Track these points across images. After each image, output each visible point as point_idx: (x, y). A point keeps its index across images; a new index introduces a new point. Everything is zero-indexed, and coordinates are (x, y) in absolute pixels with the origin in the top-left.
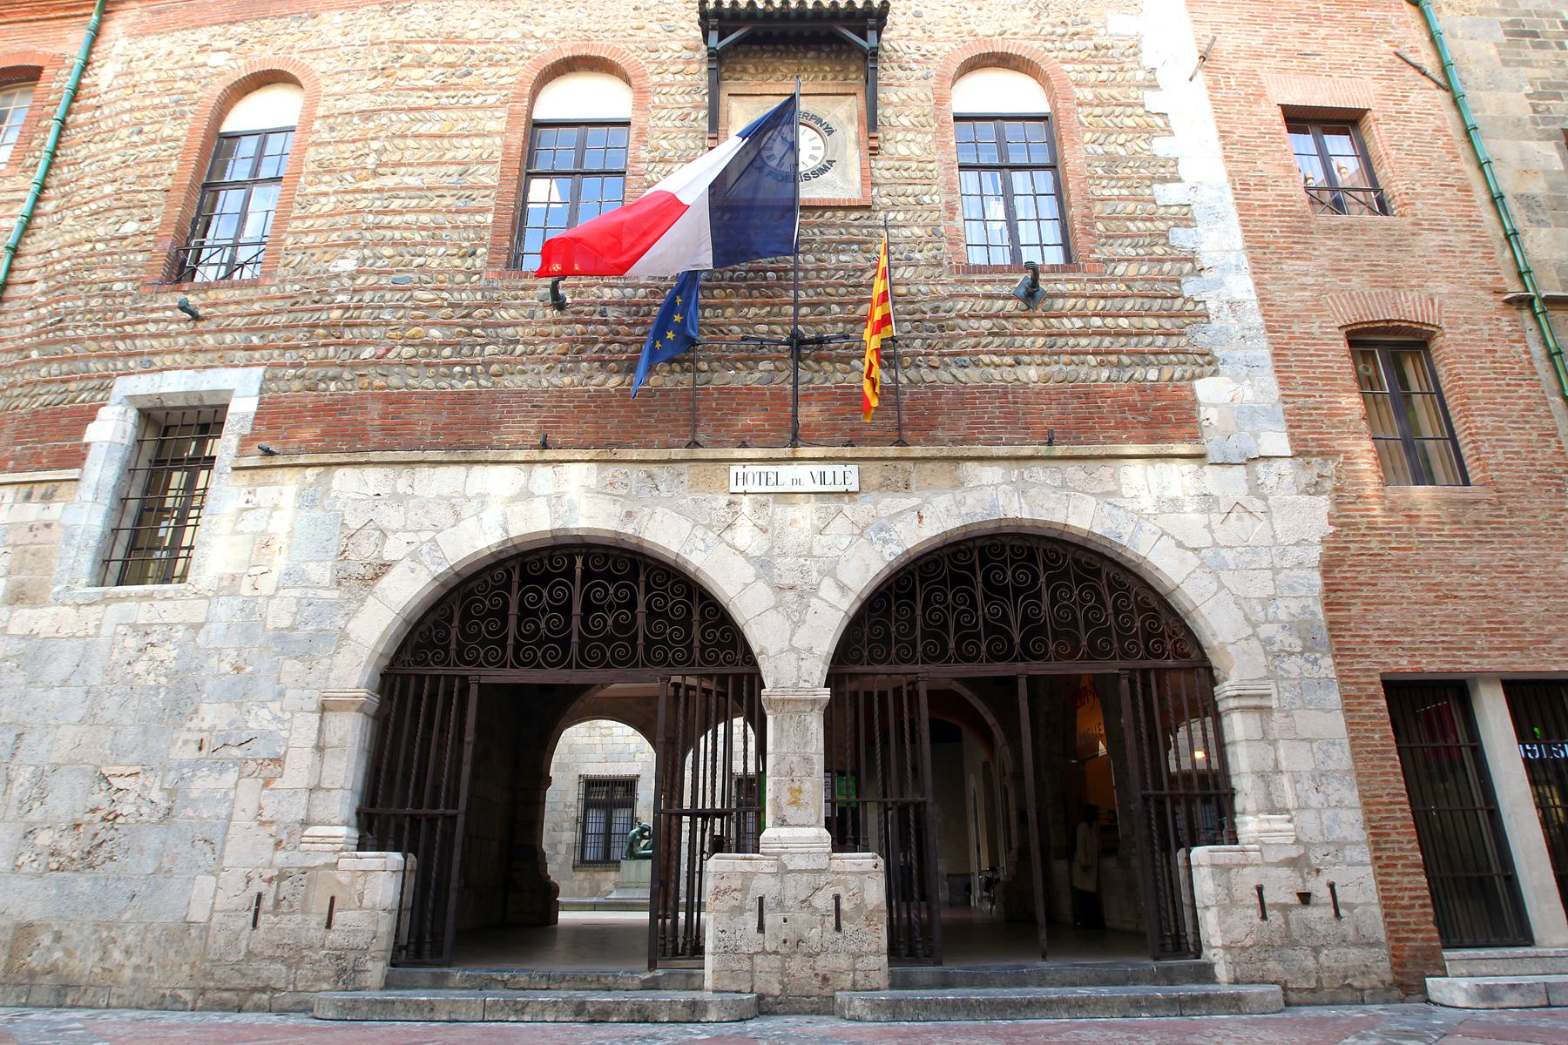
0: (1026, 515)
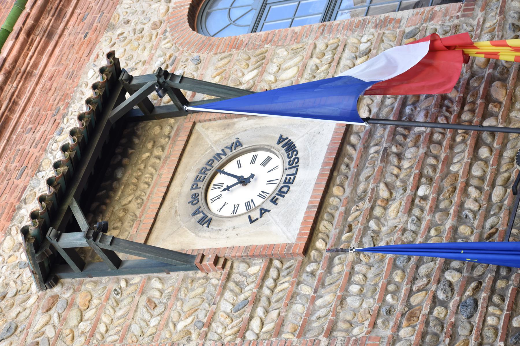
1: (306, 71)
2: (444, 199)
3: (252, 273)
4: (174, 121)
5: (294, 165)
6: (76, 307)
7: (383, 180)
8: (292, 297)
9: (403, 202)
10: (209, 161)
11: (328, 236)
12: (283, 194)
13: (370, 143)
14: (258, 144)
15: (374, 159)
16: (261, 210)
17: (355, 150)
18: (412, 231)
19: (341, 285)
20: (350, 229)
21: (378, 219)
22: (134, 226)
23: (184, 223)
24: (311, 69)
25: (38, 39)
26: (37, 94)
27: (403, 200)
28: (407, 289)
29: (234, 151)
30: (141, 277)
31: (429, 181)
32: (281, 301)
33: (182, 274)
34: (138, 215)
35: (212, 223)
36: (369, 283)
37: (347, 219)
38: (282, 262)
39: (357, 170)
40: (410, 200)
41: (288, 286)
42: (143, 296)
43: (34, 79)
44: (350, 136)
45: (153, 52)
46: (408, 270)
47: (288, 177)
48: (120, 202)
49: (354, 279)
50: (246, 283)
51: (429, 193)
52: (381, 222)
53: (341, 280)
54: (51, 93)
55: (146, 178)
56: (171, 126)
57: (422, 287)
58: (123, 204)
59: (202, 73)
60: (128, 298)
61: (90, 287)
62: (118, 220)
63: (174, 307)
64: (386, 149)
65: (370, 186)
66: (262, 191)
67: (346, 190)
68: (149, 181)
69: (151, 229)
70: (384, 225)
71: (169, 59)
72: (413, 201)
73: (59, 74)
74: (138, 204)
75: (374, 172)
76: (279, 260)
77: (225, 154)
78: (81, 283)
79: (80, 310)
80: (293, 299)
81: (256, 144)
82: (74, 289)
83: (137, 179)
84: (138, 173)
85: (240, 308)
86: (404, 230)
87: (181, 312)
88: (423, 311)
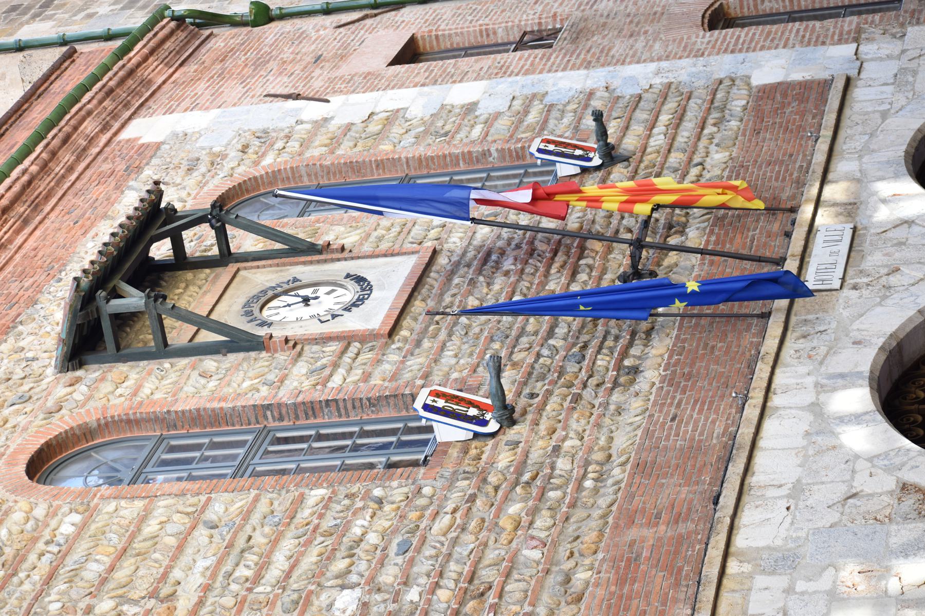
0: (904, 148)
25: (12, 220)
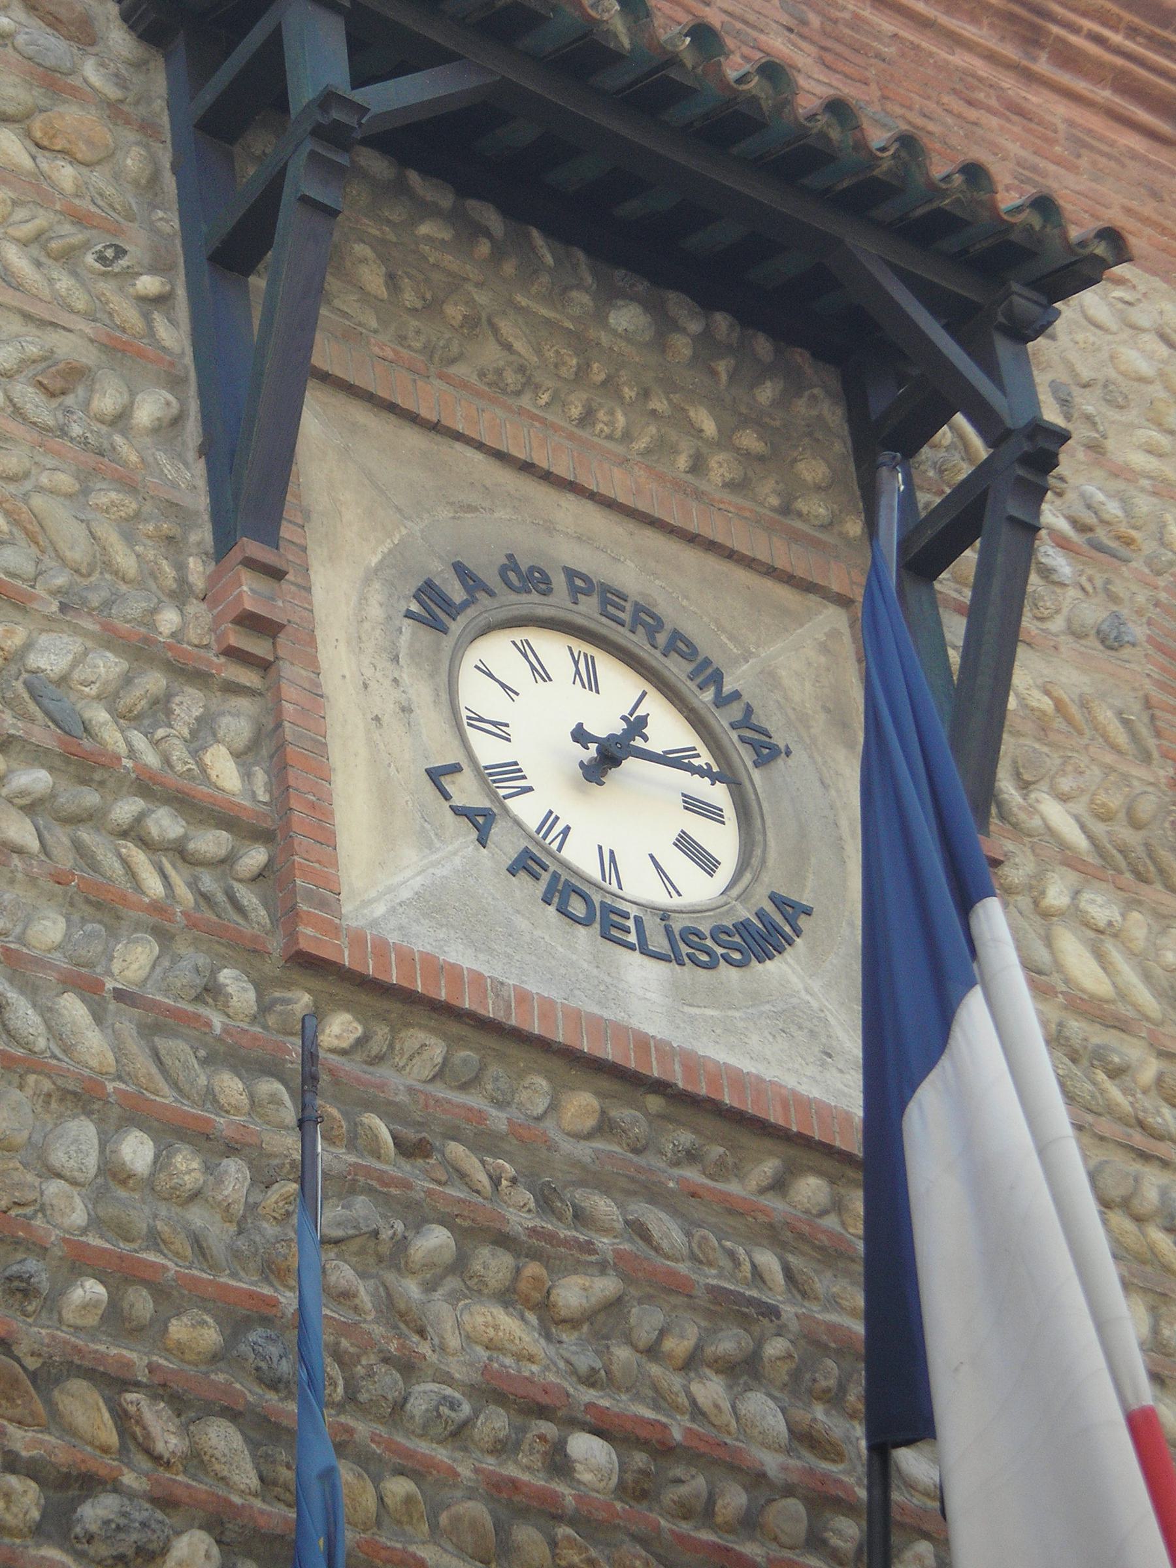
1: (1097, 1027)
2: (553, 1544)
3: (208, 759)
4: (851, 534)
5: (685, 949)
6: (44, 102)
7: (633, 1291)
8: (98, 906)
9: (535, 1368)
10: (689, 644)
11: (379, 1059)
12: (556, 900)
13: (794, 1250)
14: (769, 823)
15: (725, 1262)
16: (487, 814)
17: (763, 1191)
18: (405, 1400)
19: (153, 1097)
20: (408, 1149)
21: (459, 1265)
22: (405, 352)
23: (422, 531)
24: (1105, 1047)
26: (951, 58)
27: (547, 1368)
28: (129, 1365)
29: (734, 735)
30: (183, 353)
31: (636, 1482)
32: (82, 863)
33: (201, 502)
34: (453, 370)
35: (427, 636)
36: (163, 1213)
37: (454, 1139)
38: (259, 877)
39: (672, 1192)
40: (545, 1400)
41: (151, 893)
42: (95, 351)
43: (1010, 51)
44: (820, 1173)
45: (1145, 483)
46: (221, 1378)
47: (631, 923)
48: (504, 313)
49: (179, 1150)
50: (160, 733)
51: (579, 1482)
52: (442, 1277)
53: (176, 1100)
54: (958, 105)
55: (611, 413)
56: (831, 524)
57: (137, 1430)
58: (496, 320)
59: (1063, 649)
60: (87, 297)
61: (133, 161)
62: (428, 296)
63: (49, 462)
64: (772, 1312)
65: (605, 1240)
66: (568, 828)
67: (583, 1142)
68: (599, 426)
69: (392, 408)
70: (430, 1287)
71: (1119, 538)
72: (543, 1412)
73: (1038, 142)
74: (499, 372)
75: (668, 1258)
76: (266, 866)
77: (722, 701)
78: (147, 128)
79: (28, 116)
80: (88, 910)
81: (766, 816)
82: (122, 101)
83: (604, 383)
84: (631, 388)
85: (46, 701)
86: (408, 1367)
87: (28, 485)
88: (22, 1433)
